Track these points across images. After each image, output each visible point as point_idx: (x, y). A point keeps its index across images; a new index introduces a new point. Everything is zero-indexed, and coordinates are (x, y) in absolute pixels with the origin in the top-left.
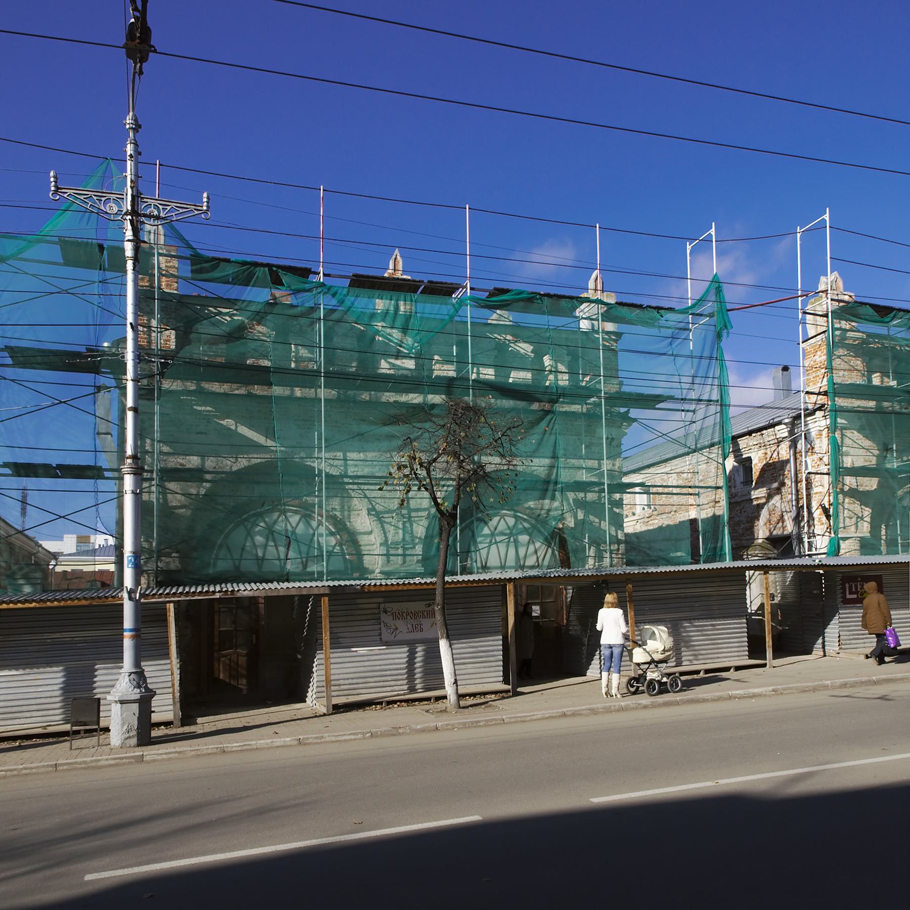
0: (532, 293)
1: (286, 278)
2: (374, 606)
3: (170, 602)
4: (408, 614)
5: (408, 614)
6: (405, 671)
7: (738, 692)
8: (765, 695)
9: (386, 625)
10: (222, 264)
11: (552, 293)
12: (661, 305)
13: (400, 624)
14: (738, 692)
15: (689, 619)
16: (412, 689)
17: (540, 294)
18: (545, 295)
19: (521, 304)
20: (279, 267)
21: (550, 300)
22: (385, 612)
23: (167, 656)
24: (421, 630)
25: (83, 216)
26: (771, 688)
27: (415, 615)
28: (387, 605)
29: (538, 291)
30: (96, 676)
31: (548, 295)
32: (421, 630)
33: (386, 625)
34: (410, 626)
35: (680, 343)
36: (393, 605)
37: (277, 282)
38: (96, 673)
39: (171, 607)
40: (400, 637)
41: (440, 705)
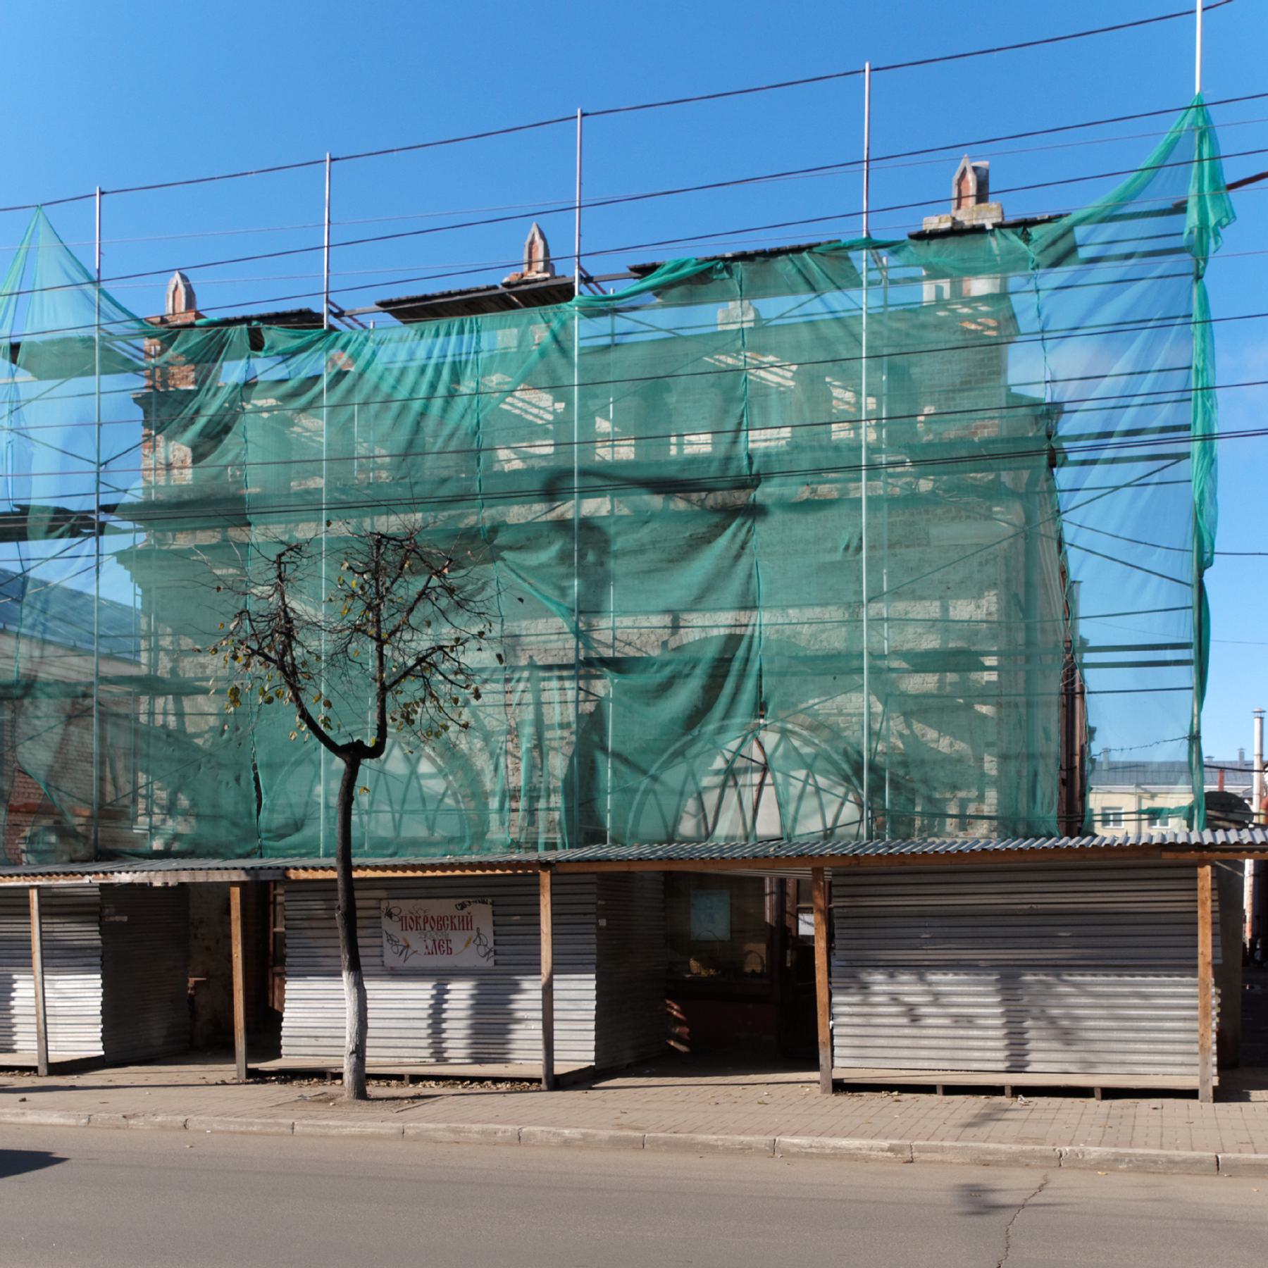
0: (707, 260)
1: (272, 334)
2: (372, 903)
3: (32, 887)
4: (426, 921)
5: (426, 921)
6: (999, 1022)
7: (796, 1140)
8: (866, 1159)
9: (390, 938)
10: (184, 332)
11: (750, 248)
12: (1029, 217)
13: (413, 938)
14: (796, 1140)
15: (1056, 968)
16: (439, 1055)
17: (724, 259)
18: (736, 258)
19: (680, 290)
20: (264, 319)
21: (751, 266)
22: (389, 914)
23: (1192, 968)
24: (450, 952)
25: (9, 301)
26: (885, 1144)
27: (439, 923)
28: (393, 903)
29: (718, 254)
30: (14, 990)
31: (743, 257)
32: (450, 952)
33: (390, 938)
34: (430, 943)
35: (91, 301)
36: (401, 903)
37: (257, 343)
38: (15, 986)
39: (34, 894)
40: (414, 962)
41: (329, 1088)
